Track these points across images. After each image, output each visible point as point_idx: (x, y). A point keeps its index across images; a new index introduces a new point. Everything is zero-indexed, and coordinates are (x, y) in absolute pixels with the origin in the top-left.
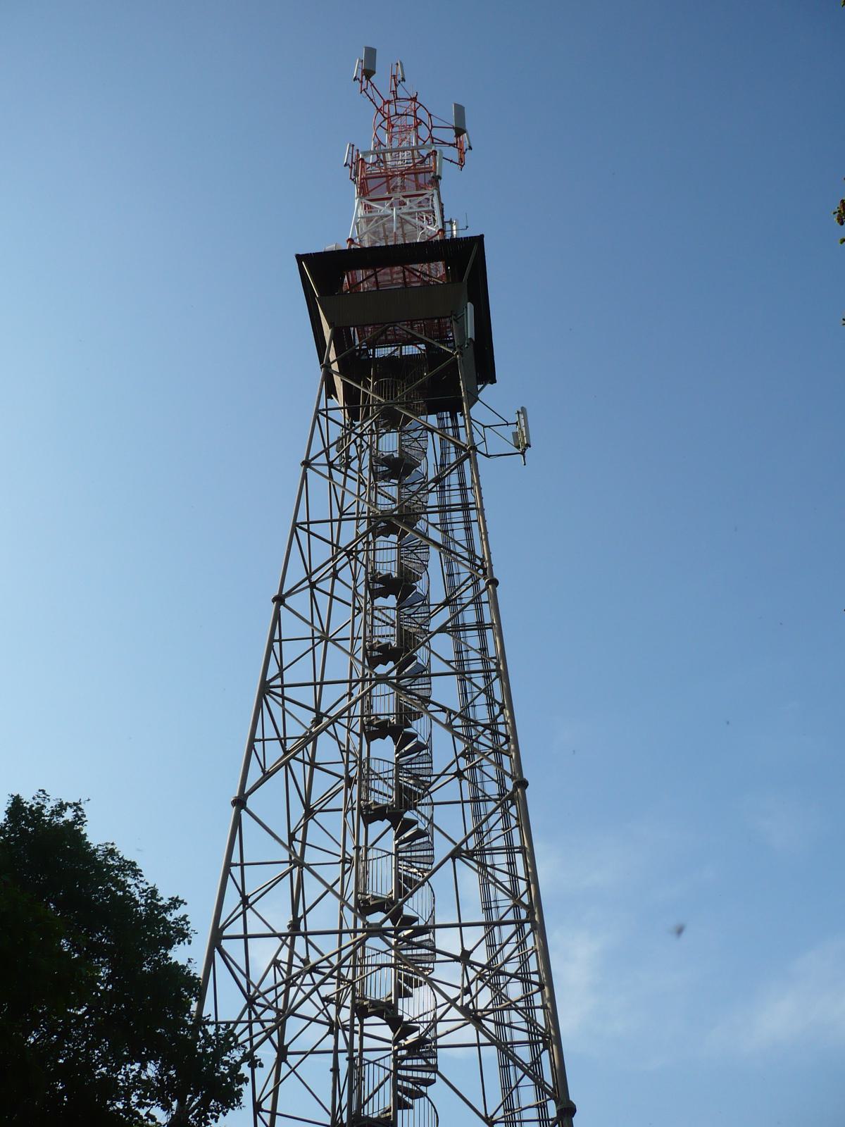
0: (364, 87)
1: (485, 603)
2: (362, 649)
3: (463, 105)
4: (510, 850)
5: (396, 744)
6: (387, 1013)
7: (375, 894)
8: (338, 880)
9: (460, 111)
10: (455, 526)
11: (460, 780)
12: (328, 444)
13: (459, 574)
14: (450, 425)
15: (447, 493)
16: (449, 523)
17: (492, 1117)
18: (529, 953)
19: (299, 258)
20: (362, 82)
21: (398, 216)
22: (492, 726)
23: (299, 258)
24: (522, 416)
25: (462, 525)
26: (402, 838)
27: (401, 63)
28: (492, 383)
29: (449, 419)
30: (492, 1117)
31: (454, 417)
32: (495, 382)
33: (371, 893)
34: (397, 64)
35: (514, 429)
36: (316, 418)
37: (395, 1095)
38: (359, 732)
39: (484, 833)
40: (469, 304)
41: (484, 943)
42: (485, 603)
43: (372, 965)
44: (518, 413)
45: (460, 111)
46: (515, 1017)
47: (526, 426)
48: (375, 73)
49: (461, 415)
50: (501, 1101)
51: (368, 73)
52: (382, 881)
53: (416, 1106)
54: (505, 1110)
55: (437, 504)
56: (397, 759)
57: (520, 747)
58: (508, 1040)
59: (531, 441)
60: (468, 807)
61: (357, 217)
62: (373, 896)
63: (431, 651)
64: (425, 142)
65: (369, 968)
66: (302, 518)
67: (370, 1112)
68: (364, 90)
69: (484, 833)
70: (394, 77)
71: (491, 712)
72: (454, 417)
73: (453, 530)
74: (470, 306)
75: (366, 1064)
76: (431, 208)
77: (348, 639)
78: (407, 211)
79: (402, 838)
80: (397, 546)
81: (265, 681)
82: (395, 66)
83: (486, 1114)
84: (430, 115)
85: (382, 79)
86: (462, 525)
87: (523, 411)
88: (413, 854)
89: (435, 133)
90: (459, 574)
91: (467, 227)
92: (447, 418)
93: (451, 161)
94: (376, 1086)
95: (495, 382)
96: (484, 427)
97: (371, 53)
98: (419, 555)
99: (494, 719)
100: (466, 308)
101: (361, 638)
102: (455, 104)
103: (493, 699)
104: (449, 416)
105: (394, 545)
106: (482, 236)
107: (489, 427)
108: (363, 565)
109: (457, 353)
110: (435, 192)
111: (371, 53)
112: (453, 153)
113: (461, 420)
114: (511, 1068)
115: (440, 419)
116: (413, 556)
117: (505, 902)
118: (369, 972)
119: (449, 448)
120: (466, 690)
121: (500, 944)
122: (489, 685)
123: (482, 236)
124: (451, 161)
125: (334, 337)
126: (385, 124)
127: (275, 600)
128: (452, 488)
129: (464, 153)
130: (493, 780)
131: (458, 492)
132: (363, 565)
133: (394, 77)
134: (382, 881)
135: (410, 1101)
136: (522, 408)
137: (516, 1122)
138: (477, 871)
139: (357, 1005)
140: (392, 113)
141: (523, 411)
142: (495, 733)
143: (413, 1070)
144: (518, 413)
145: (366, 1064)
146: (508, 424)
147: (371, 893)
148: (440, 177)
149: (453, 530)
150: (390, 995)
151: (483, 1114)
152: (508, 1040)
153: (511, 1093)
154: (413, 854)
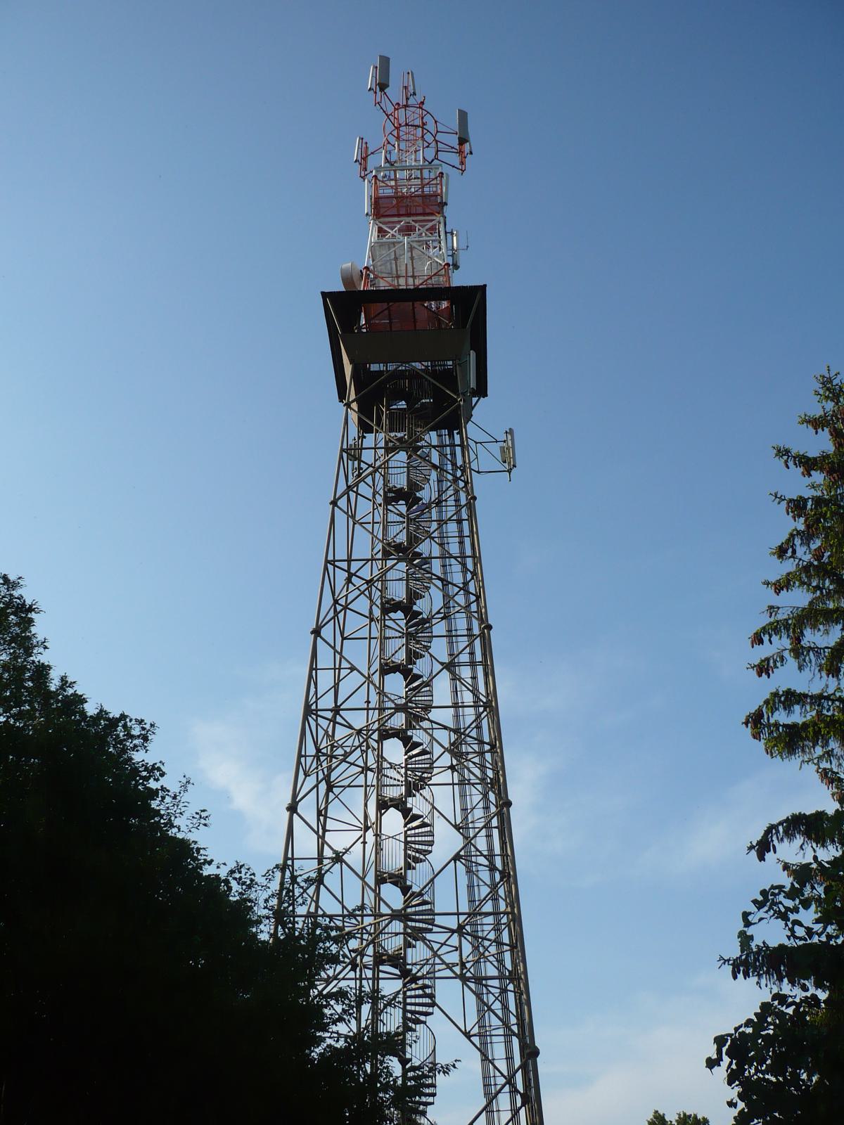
0: (378, 100)
1: (466, 537)
2: (378, 672)
3: (464, 110)
4: (473, 664)
5: (405, 747)
6: (401, 883)
7: (392, 726)
8: (361, 836)
9: (463, 116)
10: (450, 540)
11: (453, 772)
12: (335, 621)
13: (451, 565)
14: (448, 443)
15: (444, 509)
16: (454, 636)
17: (469, 1032)
18: (492, 815)
19: (324, 295)
20: (376, 93)
21: (408, 243)
22: (465, 588)
23: (324, 295)
24: (509, 437)
25: (457, 539)
26: (411, 686)
27: (412, 72)
28: (484, 397)
29: (447, 436)
30: (469, 1032)
31: (451, 435)
32: (487, 396)
33: (389, 725)
34: (409, 73)
35: (502, 444)
36: (326, 568)
37: (405, 860)
38: (377, 739)
39: (469, 811)
40: (471, 351)
41: (477, 1025)
42: (466, 537)
43: (388, 933)
44: (506, 432)
45: (463, 116)
46: (482, 860)
47: (513, 443)
48: (388, 86)
49: (457, 433)
50: (477, 1020)
51: (383, 86)
52: (398, 592)
53: (417, 868)
54: (479, 1027)
55: (439, 556)
56: (407, 570)
57: (541, 1092)
58: (483, 975)
59: (517, 462)
60: (456, 787)
61: (371, 242)
62: (390, 798)
63: (434, 807)
64: (430, 144)
65: (386, 935)
66: (330, 558)
67: (390, 869)
68: (378, 103)
69: (469, 811)
70: (406, 88)
71: (465, 577)
72: (451, 435)
73: (448, 543)
74: (473, 354)
75: (386, 839)
76: (438, 238)
77: (366, 638)
78: (417, 239)
79: (411, 686)
80: (406, 465)
81: (308, 705)
82: (406, 75)
83: (466, 1030)
84: (436, 122)
85: (395, 92)
86: (457, 539)
87: (510, 432)
88: (417, 766)
89: (440, 137)
90: (451, 565)
91: (467, 247)
92: (445, 435)
93: (453, 167)
94: (393, 652)
95: (487, 396)
96: (476, 443)
97: (385, 62)
98: (422, 471)
99: (466, 584)
100: (470, 355)
101: (374, 786)
102: (459, 110)
103: (516, 1088)
104: (447, 433)
105: (402, 465)
106: (485, 286)
107: (481, 443)
108: (379, 590)
109: (461, 400)
110: (442, 219)
111: (385, 62)
112: (455, 159)
113: (457, 440)
114: (495, 1113)
115: (440, 436)
116: (418, 472)
117: (468, 698)
118: (383, 938)
119: (446, 464)
120: (456, 688)
121: (479, 900)
122: (499, 935)
123: (485, 286)
124: (453, 167)
125: (354, 376)
126: (395, 133)
127: (331, 503)
128: (459, 633)
129: (465, 158)
130: (486, 884)
131: (464, 615)
132: (379, 590)
133: (406, 88)
134: (398, 592)
135: (414, 942)
136: (510, 429)
137: (487, 1036)
138: (471, 943)
139: (379, 876)
140: (402, 121)
141: (510, 432)
142: (467, 593)
143: (415, 844)
144: (506, 432)
145: (386, 839)
146: (497, 442)
147: (389, 725)
148: (446, 204)
149: (448, 543)
150: (403, 725)
151: (463, 1030)
152: (483, 975)
153: (484, 1015)
154: (417, 766)
